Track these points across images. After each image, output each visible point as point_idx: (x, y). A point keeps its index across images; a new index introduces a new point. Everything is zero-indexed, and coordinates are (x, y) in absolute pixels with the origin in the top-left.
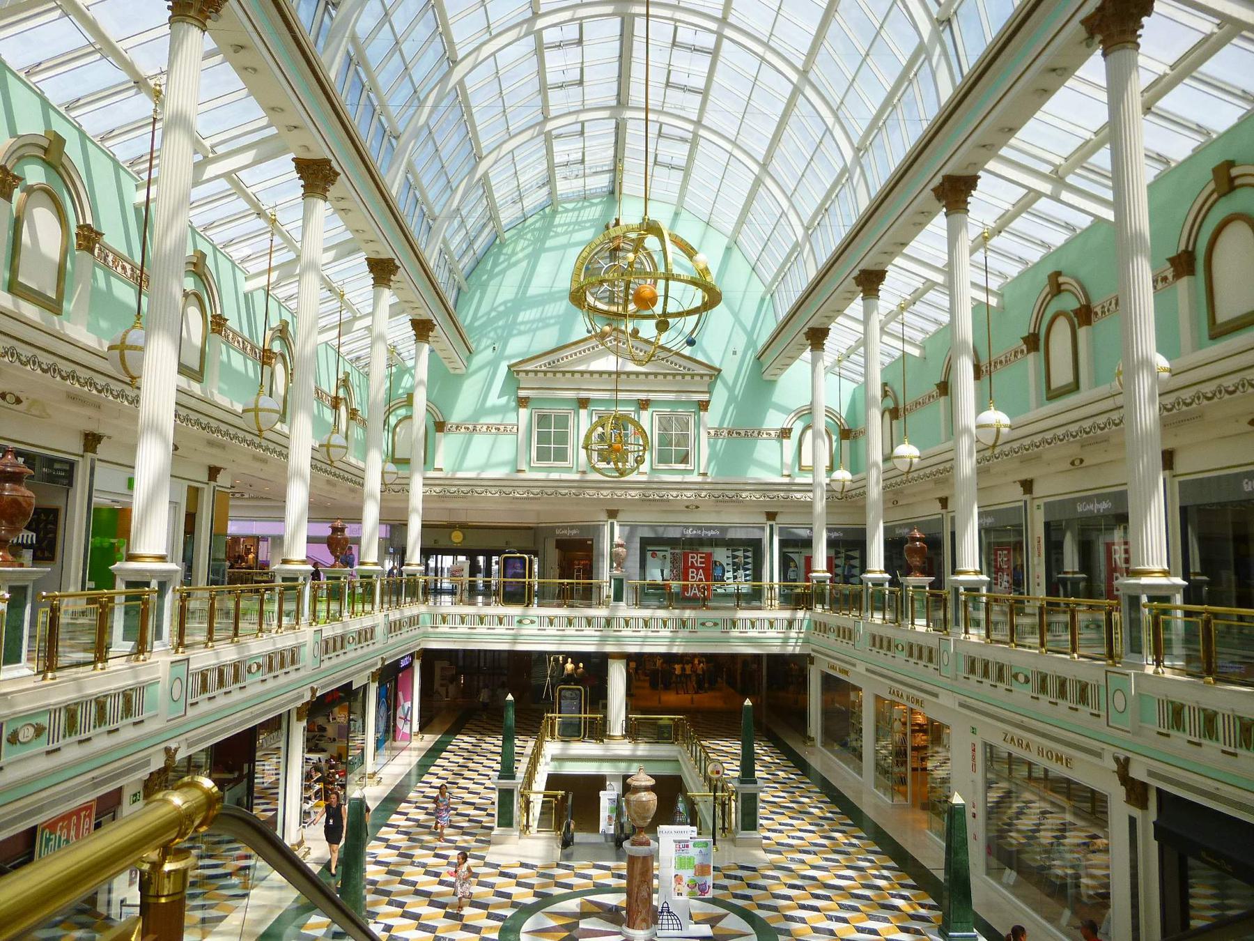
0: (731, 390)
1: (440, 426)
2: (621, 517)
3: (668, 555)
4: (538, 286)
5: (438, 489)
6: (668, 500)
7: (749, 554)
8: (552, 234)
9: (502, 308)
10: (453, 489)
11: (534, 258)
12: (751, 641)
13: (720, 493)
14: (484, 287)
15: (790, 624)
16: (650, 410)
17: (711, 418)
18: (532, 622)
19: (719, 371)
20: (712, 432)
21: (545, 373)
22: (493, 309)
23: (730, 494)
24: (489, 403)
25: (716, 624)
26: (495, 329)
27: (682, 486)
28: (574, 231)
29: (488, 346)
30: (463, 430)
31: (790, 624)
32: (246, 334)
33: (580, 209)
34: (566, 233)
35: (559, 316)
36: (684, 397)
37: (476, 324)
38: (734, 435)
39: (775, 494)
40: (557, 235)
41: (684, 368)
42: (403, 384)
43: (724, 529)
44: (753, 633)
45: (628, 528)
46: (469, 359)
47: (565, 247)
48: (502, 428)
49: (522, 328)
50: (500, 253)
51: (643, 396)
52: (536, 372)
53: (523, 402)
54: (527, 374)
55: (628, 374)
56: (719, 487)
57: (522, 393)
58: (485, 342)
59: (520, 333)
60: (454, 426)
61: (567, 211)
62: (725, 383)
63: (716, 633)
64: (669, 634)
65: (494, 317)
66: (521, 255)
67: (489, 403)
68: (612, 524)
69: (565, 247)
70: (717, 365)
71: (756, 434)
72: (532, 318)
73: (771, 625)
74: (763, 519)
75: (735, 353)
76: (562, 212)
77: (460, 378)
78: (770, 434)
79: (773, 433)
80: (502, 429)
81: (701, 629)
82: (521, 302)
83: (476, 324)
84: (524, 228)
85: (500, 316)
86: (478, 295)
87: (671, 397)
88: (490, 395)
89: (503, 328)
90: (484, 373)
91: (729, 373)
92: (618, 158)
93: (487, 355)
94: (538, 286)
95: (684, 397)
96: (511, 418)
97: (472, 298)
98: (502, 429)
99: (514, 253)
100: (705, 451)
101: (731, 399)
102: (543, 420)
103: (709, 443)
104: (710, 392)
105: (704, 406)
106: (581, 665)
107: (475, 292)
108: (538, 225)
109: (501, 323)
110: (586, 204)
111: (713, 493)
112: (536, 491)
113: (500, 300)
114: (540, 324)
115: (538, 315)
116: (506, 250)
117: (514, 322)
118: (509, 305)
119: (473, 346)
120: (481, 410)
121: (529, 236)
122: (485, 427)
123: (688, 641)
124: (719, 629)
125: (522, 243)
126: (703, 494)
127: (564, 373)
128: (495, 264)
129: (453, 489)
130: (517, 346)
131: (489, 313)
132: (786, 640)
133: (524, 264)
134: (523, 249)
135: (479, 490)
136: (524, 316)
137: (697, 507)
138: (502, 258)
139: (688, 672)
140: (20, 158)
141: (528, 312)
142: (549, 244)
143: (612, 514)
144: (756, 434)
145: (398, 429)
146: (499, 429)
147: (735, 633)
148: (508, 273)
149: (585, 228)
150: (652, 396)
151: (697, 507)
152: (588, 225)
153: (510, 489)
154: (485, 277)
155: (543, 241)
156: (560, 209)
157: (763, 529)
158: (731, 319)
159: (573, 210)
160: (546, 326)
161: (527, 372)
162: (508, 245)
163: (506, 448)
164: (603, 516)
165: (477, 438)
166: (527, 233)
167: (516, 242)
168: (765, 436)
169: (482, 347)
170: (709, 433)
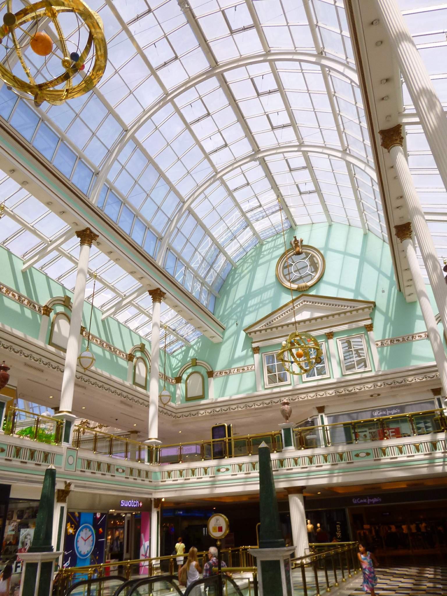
0: (386, 314)
1: (211, 374)
2: (327, 411)
3: (367, 433)
4: (257, 285)
5: (209, 411)
6: (356, 393)
7: (429, 424)
8: (261, 256)
9: (238, 302)
10: (218, 409)
11: (253, 271)
12: (400, 465)
13: (391, 381)
14: (228, 293)
15: (434, 445)
16: (335, 338)
17: (376, 335)
18: (227, 470)
19: (374, 303)
20: (379, 343)
21: (266, 330)
22: (234, 303)
23: (400, 380)
24: (236, 356)
25: (368, 454)
26: (236, 314)
27: (362, 381)
28: (273, 251)
29: (234, 324)
30: (224, 374)
31: (434, 445)
32: (23, 292)
33: (275, 240)
34: (269, 253)
35: (270, 298)
36: (354, 325)
37: (226, 313)
38: (395, 342)
39: (434, 374)
40: (264, 256)
41: (351, 307)
42: (190, 355)
43: (402, 408)
44: (402, 458)
45: (332, 418)
46: (223, 334)
47: (269, 261)
48: (246, 368)
49: (251, 309)
50: (235, 273)
51: (327, 331)
52: (260, 331)
53: (256, 350)
54: (255, 333)
55: (316, 319)
56: (389, 377)
57: (255, 345)
58: (231, 322)
59: (250, 312)
60: (219, 373)
61: (268, 242)
62: (381, 312)
63: (370, 461)
64: (328, 467)
65: (235, 307)
66: (246, 272)
67: (236, 356)
68: (322, 416)
69: (269, 261)
70: (372, 300)
71: (410, 338)
72: (255, 302)
73: (418, 449)
74: (431, 395)
75: (383, 291)
76: (266, 244)
77: (219, 345)
78: (421, 336)
79: (423, 335)
80: (246, 369)
81: (356, 459)
82: (249, 295)
83: (226, 313)
84: (246, 258)
85: (238, 306)
86: (225, 298)
87: (345, 327)
88: (237, 351)
89: (240, 312)
90: (232, 338)
91: (381, 304)
92: (279, 196)
93: (233, 329)
94: (257, 285)
95: (354, 325)
96: (250, 362)
97: (222, 300)
98: (246, 369)
99: (242, 272)
100: (376, 357)
101: (387, 320)
102: (271, 358)
103: (378, 351)
104: (372, 319)
105: (370, 328)
106: (318, 525)
107: (224, 296)
108: (253, 254)
109: (239, 310)
110: (278, 236)
111: (387, 382)
112: (267, 402)
113: (237, 298)
114: (261, 305)
115: (259, 301)
116: (239, 271)
117: (246, 307)
118: (242, 299)
119: (225, 326)
120: (232, 361)
121: (249, 261)
122: (236, 370)
123: (345, 471)
124: (371, 458)
125: (246, 265)
126: (379, 384)
127: (277, 327)
128: (233, 279)
129: (218, 409)
130: (248, 320)
131: (232, 306)
132: (432, 461)
133: (248, 276)
134: (247, 268)
135: (233, 407)
136: (251, 303)
137: (379, 395)
138: (236, 276)
139: (414, 530)
140: (54, 305)
141: (253, 300)
142: (261, 261)
143: (321, 409)
144: (410, 338)
145: (188, 381)
146: (244, 369)
147: (385, 459)
148: (240, 282)
149: (280, 248)
150: (334, 329)
151: (379, 395)
152: (280, 246)
153: (252, 403)
154: (228, 288)
155: (257, 261)
156: (265, 243)
157: (433, 403)
158: (377, 273)
159: (272, 241)
160: (265, 305)
161: (255, 332)
162: (239, 268)
163: (248, 380)
164: (315, 412)
165: (231, 378)
166: (248, 260)
167: (243, 265)
168: (417, 338)
169: (230, 324)
170: (377, 345)
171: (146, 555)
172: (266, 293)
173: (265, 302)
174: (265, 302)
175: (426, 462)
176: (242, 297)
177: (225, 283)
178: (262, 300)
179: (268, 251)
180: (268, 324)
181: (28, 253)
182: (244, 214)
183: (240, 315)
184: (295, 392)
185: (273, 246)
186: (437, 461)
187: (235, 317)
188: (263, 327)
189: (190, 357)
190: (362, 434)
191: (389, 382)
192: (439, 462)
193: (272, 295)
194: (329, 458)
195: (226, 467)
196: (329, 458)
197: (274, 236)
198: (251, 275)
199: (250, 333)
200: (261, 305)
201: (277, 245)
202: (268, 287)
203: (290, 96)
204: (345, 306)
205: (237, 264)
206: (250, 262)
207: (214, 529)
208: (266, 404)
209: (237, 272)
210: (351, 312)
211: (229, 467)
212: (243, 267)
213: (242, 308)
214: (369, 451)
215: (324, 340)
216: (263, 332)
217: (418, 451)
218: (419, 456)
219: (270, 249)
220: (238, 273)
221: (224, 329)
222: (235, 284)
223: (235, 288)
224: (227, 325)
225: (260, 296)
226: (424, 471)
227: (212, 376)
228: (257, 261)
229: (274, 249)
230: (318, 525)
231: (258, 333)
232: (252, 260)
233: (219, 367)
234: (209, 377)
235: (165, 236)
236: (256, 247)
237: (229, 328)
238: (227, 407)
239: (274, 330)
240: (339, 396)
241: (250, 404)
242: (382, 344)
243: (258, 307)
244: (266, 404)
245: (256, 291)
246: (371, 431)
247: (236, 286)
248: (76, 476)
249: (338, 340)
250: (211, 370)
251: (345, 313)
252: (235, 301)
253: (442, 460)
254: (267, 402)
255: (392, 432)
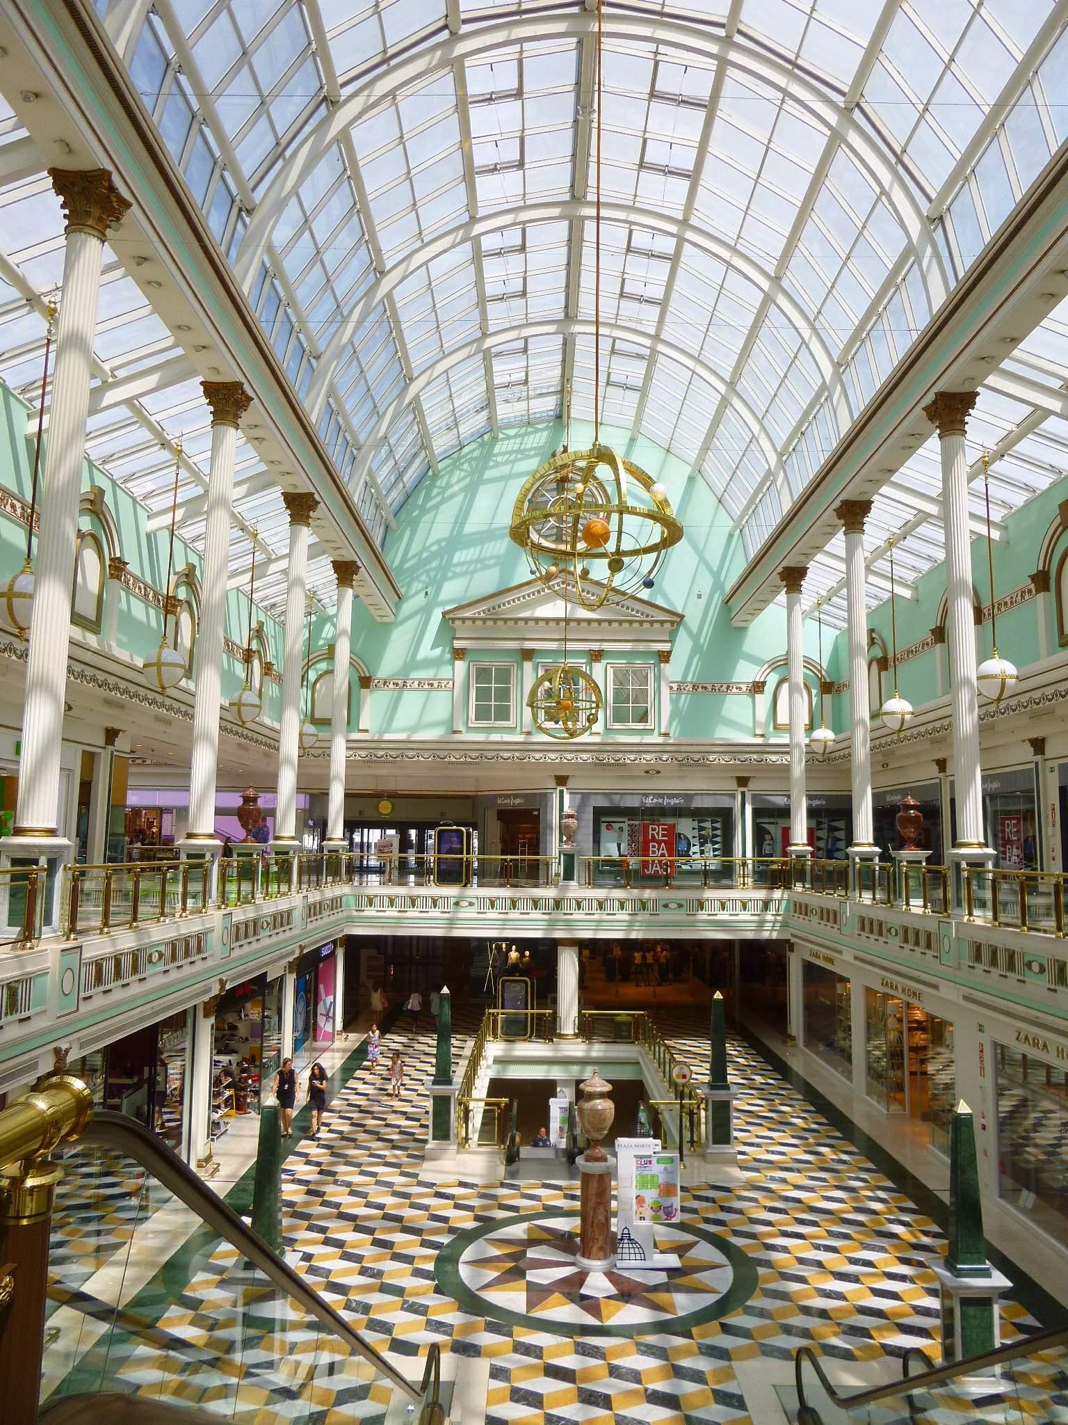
0: (695, 638)
1: (366, 682)
2: (570, 784)
3: (625, 826)
5: (363, 753)
7: (718, 825)
9: (435, 548)
10: (381, 753)
11: (471, 491)
14: (415, 523)
15: (766, 905)
16: (604, 662)
17: (673, 671)
18: (471, 904)
19: (682, 617)
20: (675, 686)
21: (484, 620)
22: (425, 549)
23: (696, 757)
25: (680, 906)
26: (428, 572)
27: (641, 749)
28: (516, 460)
29: (420, 591)
30: (391, 686)
34: (507, 462)
35: (498, 557)
36: (642, 647)
37: (406, 566)
38: (700, 690)
40: (497, 464)
41: (642, 614)
42: (324, 635)
43: (688, 797)
44: (723, 916)
47: (505, 479)
49: (458, 570)
50: (432, 486)
51: (595, 646)
52: (474, 620)
53: (459, 654)
57: (458, 644)
58: (416, 586)
59: (456, 576)
61: (508, 437)
63: (680, 916)
64: (627, 918)
66: (456, 488)
68: (561, 792)
69: (505, 479)
70: (680, 611)
74: (733, 785)
75: (699, 596)
76: (503, 439)
77: (388, 627)
78: (740, 689)
79: (744, 687)
81: (663, 911)
82: (456, 541)
83: (406, 566)
84: (459, 458)
85: (433, 556)
86: (408, 533)
87: (628, 646)
91: (693, 618)
95: (642, 647)
96: (445, 672)
97: (401, 537)
99: (449, 486)
101: (696, 648)
102: (483, 674)
104: (671, 641)
105: (665, 657)
106: (527, 953)
107: (404, 531)
108: (475, 454)
109: (434, 565)
110: (530, 430)
112: (474, 754)
114: (479, 566)
118: (443, 544)
119: (402, 591)
120: (412, 663)
121: (466, 466)
122: (416, 683)
123: (648, 925)
125: (458, 475)
128: (428, 498)
129: (381, 753)
130: (452, 591)
131: (420, 553)
132: (761, 923)
133: (460, 498)
135: (410, 753)
136: (459, 557)
137: (658, 772)
138: (435, 491)
141: (465, 552)
142: (488, 474)
143: (561, 780)
145: (318, 685)
146: (432, 685)
147: (702, 915)
149: (529, 457)
150: (606, 646)
151: (658, 772)
152: (532, 453)
154: (416, 513)
156: (501, 436)
157: (733, 796)
159: (516, 436)
161: (463, 620)
163: (440, 705)
164: (552, 784)
165: (407, 695)
167: (451, 473)
168: (734, 690)
169: (412, 592)
170: (671, 688)
171: (328, 1014)
172: (492, 544)
173: (486, 562)
174: (486, 562)
175: (755, 924)
176: (444, 540)
177: (410, 501)
178: (482, 556)
179: (506, 457)
180: (489, 610)
181: (91, 436)
182: (490, 389)
183: (436, 576)
184: (526, 747)
185: (516, 447)
186: (767, 924)
187: (424, 577)
188: (479, 613)
189: (325, 639)
190: (616, 826)
191: (680, 757)
192: (768, 926)
193: (502, 551)
194: (628, 905)
195: (469, 900)
196: (628, 905)
197: (521, 427)
198: (465, 497)
199: (453, 620)
200: (479, 566)
201: (525, 450)
202: (497, 533)
203: (680, 273)
204: (638, 612)
205: (440, 466)
206: (466, 471)
207: (678, 1076)
208: (470, 757)
209: (438, 484)
210: (641, 623)
211: (474, 901)
212: (450, 477)
213: (440, 564)
214: (684, 903)
215: (584, 661)
216: (479, 623)
217: (745, 909)
218: (745, 916)
219: (511, 453)
220: (440, 487)
221: (400, 598)
222: (431, 509)
223: (427, 518)
224: (407, 591)
225: (479, 548)
226: (750, 935)
227: (368, 687)
228: (482, 474)
229: (519, 456)
230: (527, 953)
231: (468, 623)
232: (470, 465)
233: (383, 672)
234: (362, 687)
235: (368, 443)
236: (483, 440)
237: (413, 596)
238: (399, 752)
239: (500, 623)
240: (596, 764)
241: (442, 754)
242: (679, 689)
243: (472, 568)
244: (470, 757)
245: (472, 534)
246: (631, 822)
247: (433, 513)
248: (310, 931)
249: (609, 666)
250: (367, 675)
251: (631, 622)
252: (427, 544)
253: (771, 924)
254: (474, 754)
255: (663, 830)
